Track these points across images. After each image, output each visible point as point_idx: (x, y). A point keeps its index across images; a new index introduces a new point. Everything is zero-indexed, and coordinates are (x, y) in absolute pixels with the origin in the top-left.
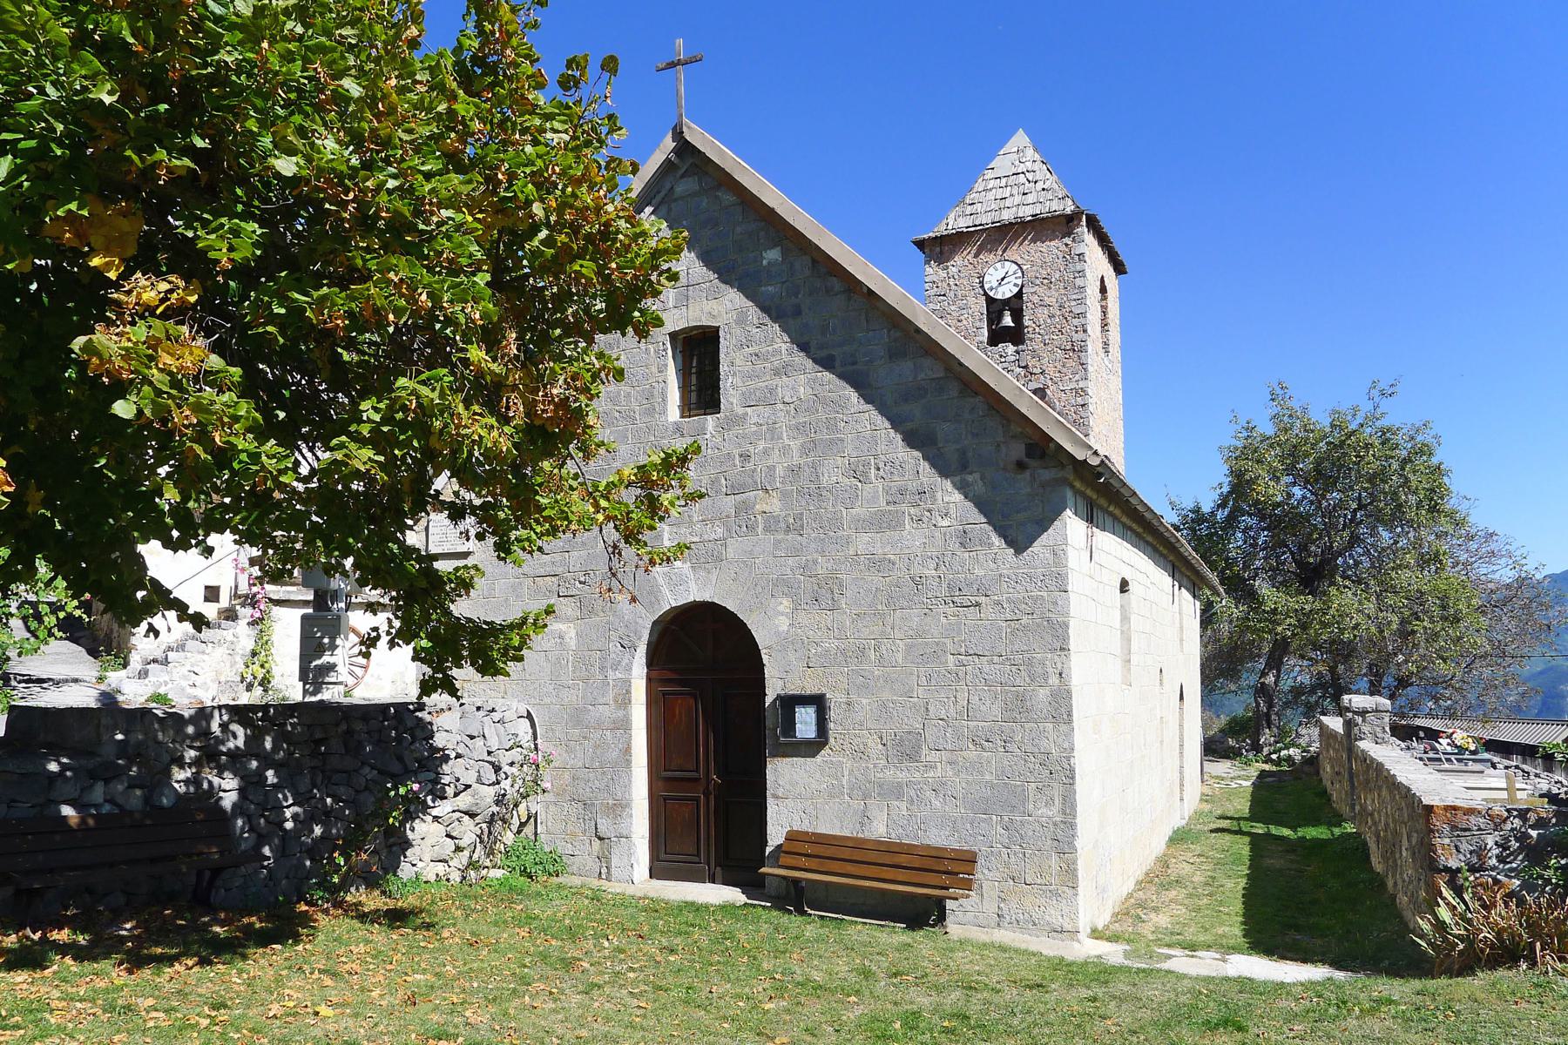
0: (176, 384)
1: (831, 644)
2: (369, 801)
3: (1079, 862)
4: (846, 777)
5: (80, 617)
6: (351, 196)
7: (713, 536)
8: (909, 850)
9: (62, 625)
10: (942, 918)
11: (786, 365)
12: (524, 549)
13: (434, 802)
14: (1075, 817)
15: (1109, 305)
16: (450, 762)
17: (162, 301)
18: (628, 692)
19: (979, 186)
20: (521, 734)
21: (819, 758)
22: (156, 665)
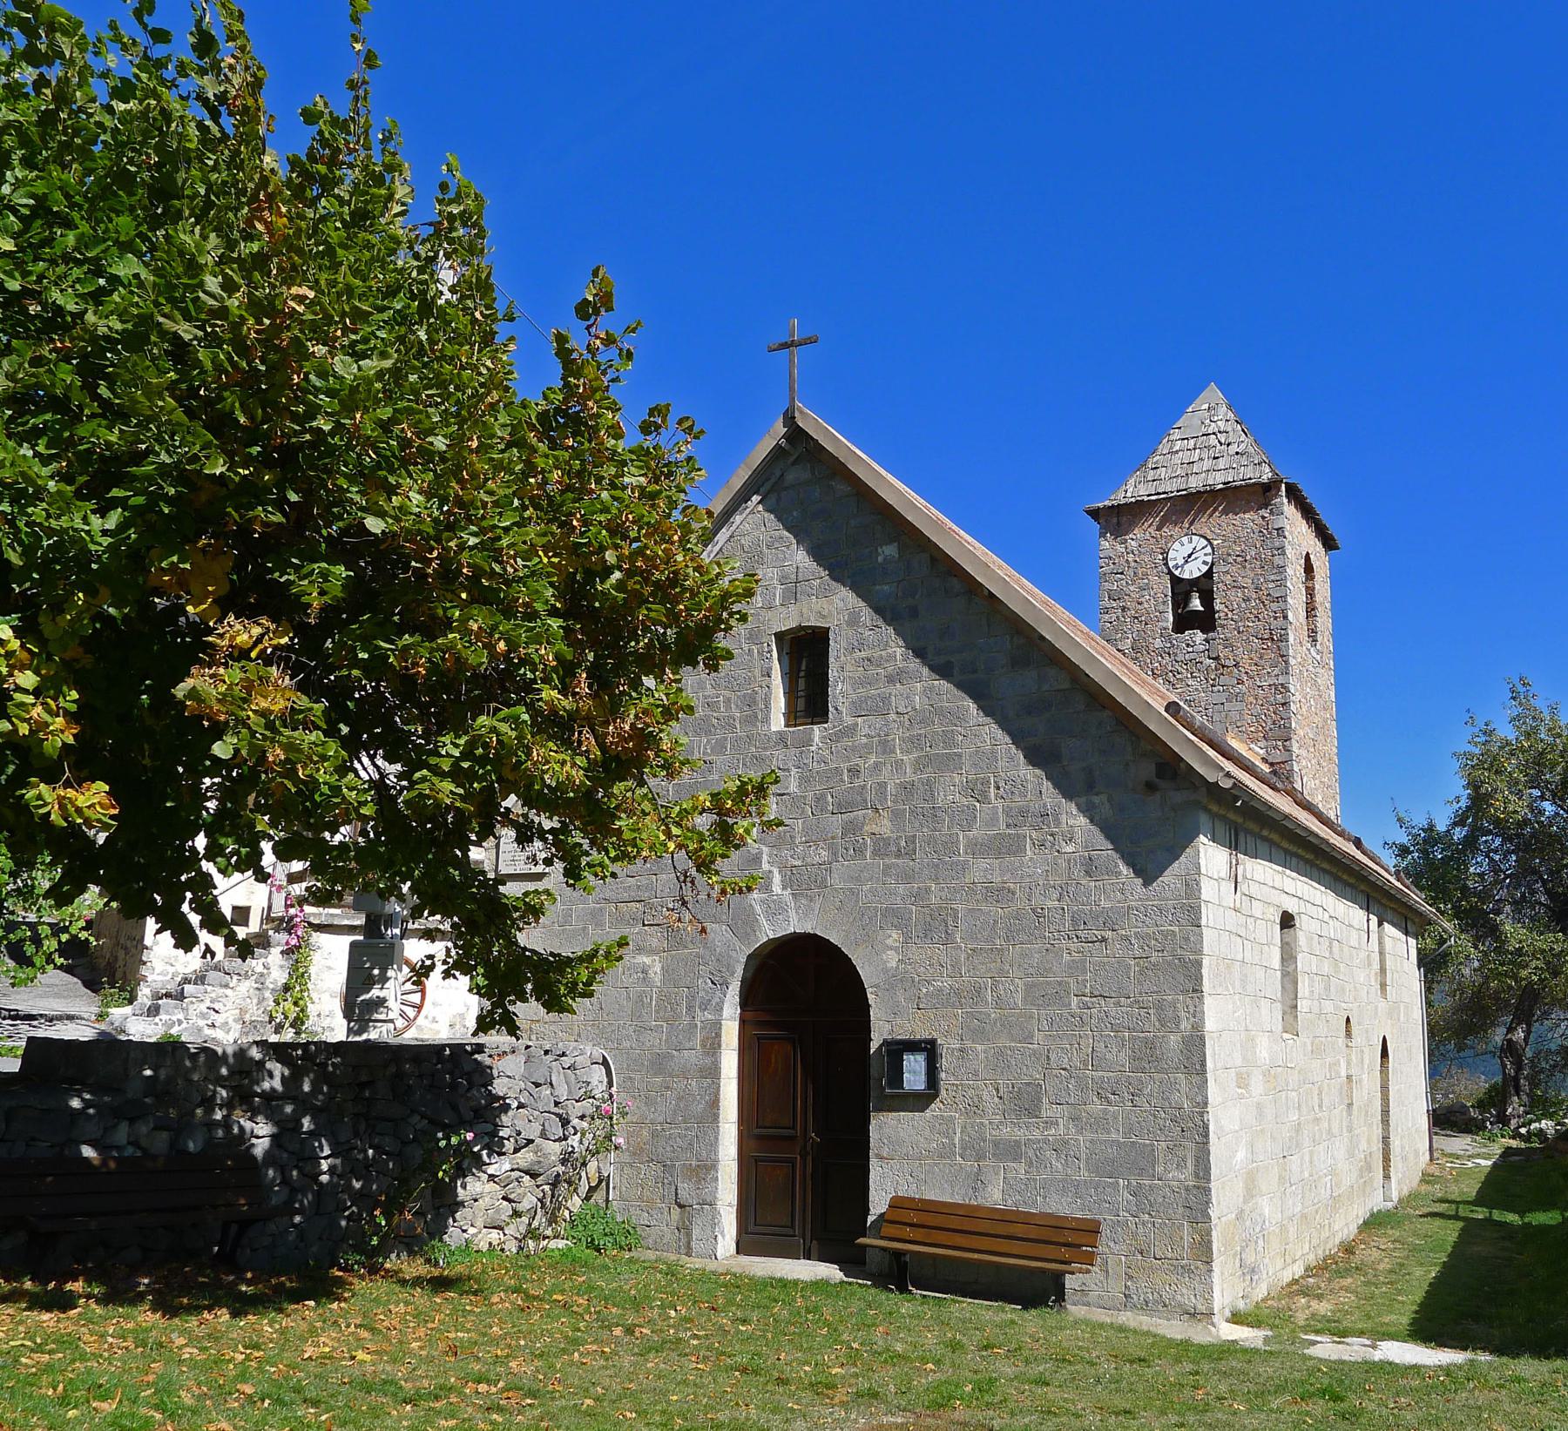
0: (270, 726)
1: (945, 983)
2: (417, 1154)
3: (1214, 1233)
4: (958, 1135)
5: (87, 939)
6: (435, 554)
7: (817, 859)
8: (1026, 1219)
9: (63, 950)
10: (1061, 1297)
11: (901, 672)
12: (596, 875)
13: (489, 1156)
14: (1209, 1181)
15: (1317, 587)
16: (510, 1113)
17: (255, 645)
18: (718, 1035)
19: (1164, 448)
20: (595, 1082)
21: (928, 1113)
22: (169, 1001)
